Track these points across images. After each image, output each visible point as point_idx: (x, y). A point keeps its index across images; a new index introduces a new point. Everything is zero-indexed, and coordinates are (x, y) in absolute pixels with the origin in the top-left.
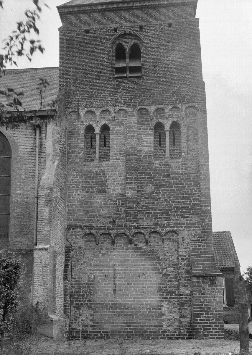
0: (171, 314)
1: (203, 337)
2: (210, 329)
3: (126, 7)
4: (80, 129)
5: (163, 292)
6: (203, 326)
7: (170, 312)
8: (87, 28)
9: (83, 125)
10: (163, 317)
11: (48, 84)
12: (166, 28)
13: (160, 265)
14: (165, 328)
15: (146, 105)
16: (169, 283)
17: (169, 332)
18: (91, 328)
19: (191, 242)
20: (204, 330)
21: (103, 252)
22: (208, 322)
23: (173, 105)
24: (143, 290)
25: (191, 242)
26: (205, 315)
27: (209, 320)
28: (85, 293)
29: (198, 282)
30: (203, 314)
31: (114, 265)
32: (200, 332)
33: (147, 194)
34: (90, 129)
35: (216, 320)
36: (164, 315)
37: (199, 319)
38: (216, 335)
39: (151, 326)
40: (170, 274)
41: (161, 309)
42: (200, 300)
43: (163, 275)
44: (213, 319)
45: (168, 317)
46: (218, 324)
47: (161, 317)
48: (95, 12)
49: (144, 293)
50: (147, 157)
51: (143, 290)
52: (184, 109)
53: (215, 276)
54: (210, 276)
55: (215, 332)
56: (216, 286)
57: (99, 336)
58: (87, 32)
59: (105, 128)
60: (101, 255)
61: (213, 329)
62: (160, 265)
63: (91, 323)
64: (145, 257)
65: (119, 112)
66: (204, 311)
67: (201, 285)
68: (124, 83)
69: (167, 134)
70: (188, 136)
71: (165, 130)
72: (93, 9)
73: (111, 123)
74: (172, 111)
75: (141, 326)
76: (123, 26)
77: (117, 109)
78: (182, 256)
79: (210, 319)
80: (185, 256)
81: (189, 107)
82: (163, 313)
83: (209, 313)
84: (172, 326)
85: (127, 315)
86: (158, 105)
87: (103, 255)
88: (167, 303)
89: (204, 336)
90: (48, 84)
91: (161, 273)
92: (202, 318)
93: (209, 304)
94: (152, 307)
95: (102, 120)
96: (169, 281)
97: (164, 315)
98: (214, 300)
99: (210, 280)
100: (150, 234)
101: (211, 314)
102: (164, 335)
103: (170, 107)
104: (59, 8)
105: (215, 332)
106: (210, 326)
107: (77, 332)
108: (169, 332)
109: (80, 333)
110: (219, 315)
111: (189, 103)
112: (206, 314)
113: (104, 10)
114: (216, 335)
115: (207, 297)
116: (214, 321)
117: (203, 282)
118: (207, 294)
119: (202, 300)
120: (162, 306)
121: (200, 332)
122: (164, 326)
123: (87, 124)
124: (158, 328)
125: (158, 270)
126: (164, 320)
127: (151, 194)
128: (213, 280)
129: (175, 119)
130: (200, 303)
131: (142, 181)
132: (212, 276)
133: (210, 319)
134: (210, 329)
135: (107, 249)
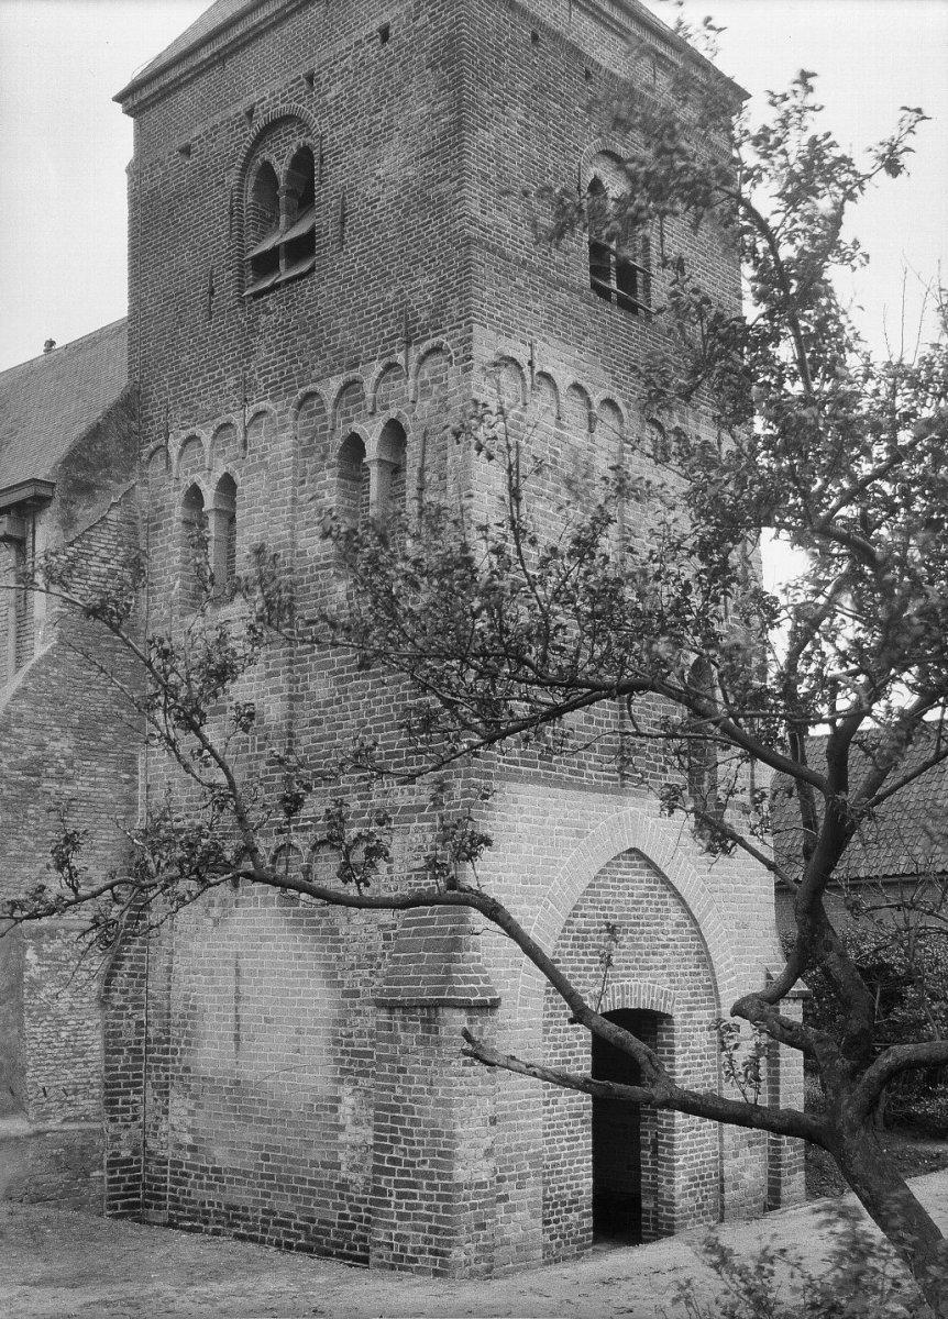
0: (359, 1129)
1: (395, 1221)
2: (414, 1196)
3: (267, 18)
4: (173, 506)
5: (343, 1052)
6: (398, 1184)
7: (357, 1123)
8: (179, 143)
9: (179, 489)
10: (342, 1138)
11: (814, 75)
12: (372, 51)
13: (339, 958)
14: (344, 1173)
15: (317, 380)
16: (359, 1019)
17: (354, 1188)
18: (189, 1154)
19: (409, 877)
20: (401, 1196)
21: (215, 912)
22: (411, 1169)
23: (386, 360)
24: (297, 1040)
25: (409, 877)
26: (402, 1146)
27: (412, 1164)
28: (179, 1043)
29: (390, 1026)
30: (395, 1140)
31: (238, 955)
32: (388, 1204)
33: (317, 706)
34: (194, 496)
35: (435, 1164)
36: (342, 1128)
37: (386, 1155)
38: (429, 1218)
39: (314, 1164)
40: (361, 988)
41: (334, 1109)
42: (392, 1089)
43: (346, 994)
44: (424, 1162)
45: (351, 1139)
46: (436, 1181)
47: (336, 1137)
48: (200, 74)
49: (298, 1051)
50: (319, 572)
51: (297, 1040)
52: (413, 365)
53: (436, 1007)
54: (422, 1007)
55: (428, 1208)
56: (438, 1043)
57: (205, 1181)
58: (186, 151)
59: (228, 486)
60: (210, 922)
61: (423, 1197)
62: (339, 958)
63: (188, 1139)
64: (305, 931)
65: (257, 422)
66: (402, 1130)
67: (398, 1038)
68: (267, 312)
69: (374, 470)
70: (422, 471)
71: (365, 460)
72: (193, 68)
73: (238, 467)
74: (388, 380)
75: (292, 1161)
76: (267, 95)
77: (250, 411)
78: (386, 926)
79: (417, 1160)
80: (394, 926)
81: (430, 352)
82: (341, 1122)
83: (415, 1138)
84: (361, 1169)
85: (261, 1120)
86: (348, 368)
87: (216, 922)
88: (350, 1090)
89: (398, 1218)
90: (814, 75)
91: (341, 984)
92: (394, 1155)
93: (416, 1106)
94: (317, 1100)
95: (220, 461)
96: (358, 1013)
97: (342, 1128)
98: (430, 1092)
99: (423, 1020)
100: (314, 848)
101: (421, 1143)
102: (342, 1197)
103: (378, 367)
104: (120, 98)
105: (428, 1208)
106: (414, 1185)
107: (159, 1163)
108: (354, 1188)
109: (168, 1167)
110: (442, 1149)
111: (428, 338)
112: (406, 1141)
113: (221, 58)
114: (429, 1218)
115: (410, 1080)
116: (426, 1168)
117: (405, 1028)
118: (414, 1071)
119: (399, 1092)
120: (338, 1100)
121: (388, 1204)
122: (344, 1168)
123: (186, 483)
124: (329, 1172)
125: (331, 977)
126: (342, 1146)
127: (328, 704)
128: (429, 1021)
129: (393, 413)
130: (393, 1102)
131: (305, 660)
132: (428, 1007)
133: (417, 1160)
134: (414, 1196)
135: (224, 902)
